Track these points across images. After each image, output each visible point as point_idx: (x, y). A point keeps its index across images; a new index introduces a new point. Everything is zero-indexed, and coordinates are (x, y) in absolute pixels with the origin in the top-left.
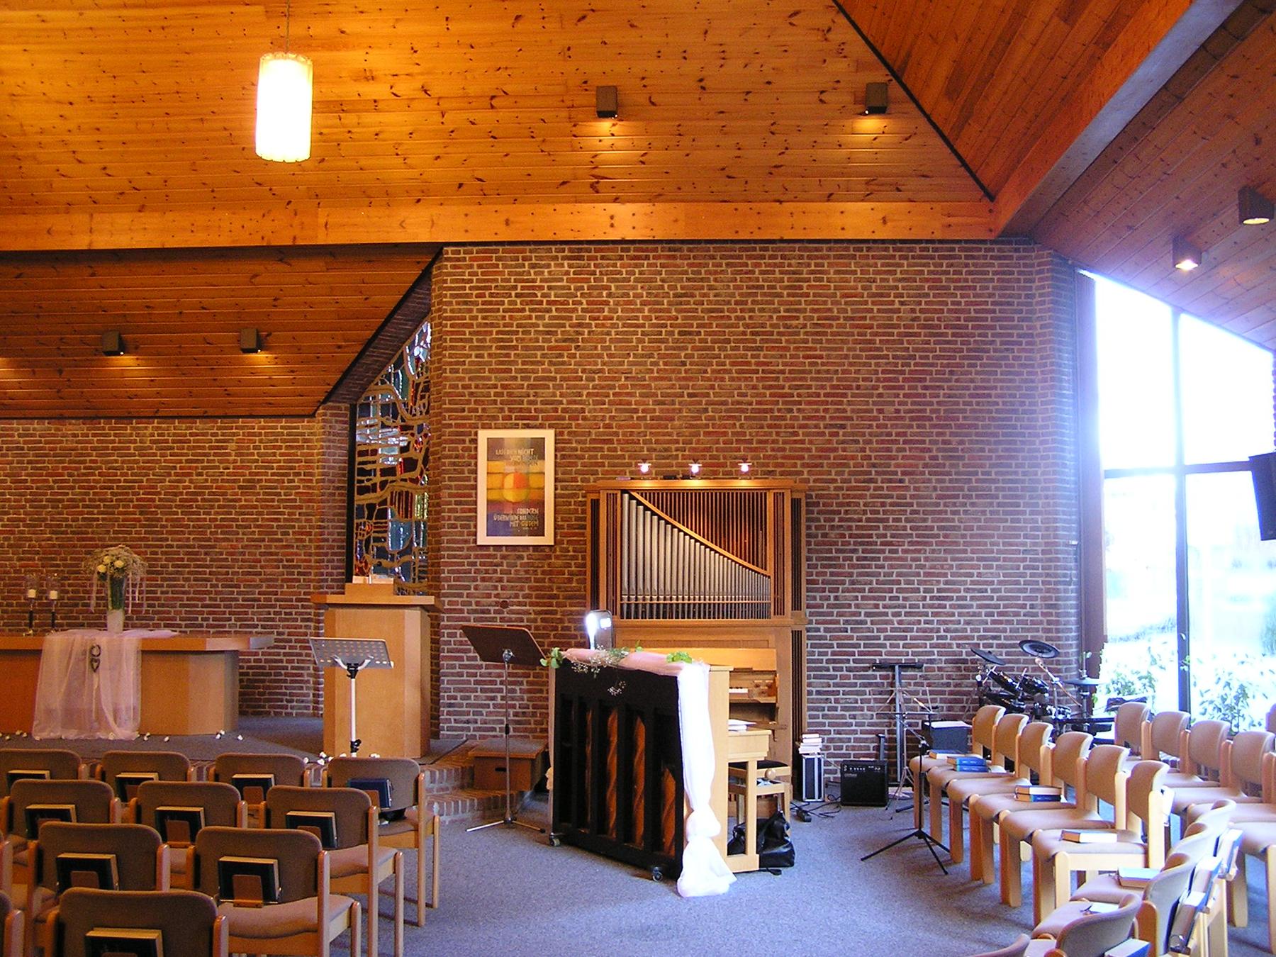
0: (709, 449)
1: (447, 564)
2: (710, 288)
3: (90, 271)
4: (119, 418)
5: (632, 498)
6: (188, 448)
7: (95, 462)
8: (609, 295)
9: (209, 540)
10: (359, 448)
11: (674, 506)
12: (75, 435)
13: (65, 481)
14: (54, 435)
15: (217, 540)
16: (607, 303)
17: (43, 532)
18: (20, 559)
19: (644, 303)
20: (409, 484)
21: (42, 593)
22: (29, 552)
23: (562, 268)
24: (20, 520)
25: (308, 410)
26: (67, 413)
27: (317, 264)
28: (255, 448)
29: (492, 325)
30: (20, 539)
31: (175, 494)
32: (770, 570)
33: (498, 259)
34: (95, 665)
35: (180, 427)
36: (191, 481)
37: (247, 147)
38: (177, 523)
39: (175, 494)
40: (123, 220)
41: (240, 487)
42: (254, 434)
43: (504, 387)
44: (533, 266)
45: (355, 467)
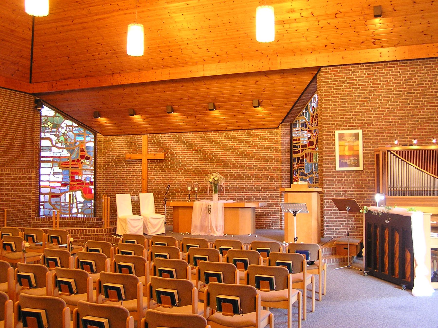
3: (204, 83)
5: (391, 153)
7: (207, 145)
8: (381, 81)
9: (245, 170)
11: (407, 156)
12: (201, 137)
13: (198, 152)
14: (194, 137)
18: (185, 178)
19: (393, 83)
23: (362, 73)
25: (276, 126)
26: (197, 130)
27: (278, 76)
30: (185, 171)
31: (233, 156)
36: (238, 151)
39: (233, 156)
41: (254, 153)
42: (258, 135)
43: (344, 115)
44: (353, 73)
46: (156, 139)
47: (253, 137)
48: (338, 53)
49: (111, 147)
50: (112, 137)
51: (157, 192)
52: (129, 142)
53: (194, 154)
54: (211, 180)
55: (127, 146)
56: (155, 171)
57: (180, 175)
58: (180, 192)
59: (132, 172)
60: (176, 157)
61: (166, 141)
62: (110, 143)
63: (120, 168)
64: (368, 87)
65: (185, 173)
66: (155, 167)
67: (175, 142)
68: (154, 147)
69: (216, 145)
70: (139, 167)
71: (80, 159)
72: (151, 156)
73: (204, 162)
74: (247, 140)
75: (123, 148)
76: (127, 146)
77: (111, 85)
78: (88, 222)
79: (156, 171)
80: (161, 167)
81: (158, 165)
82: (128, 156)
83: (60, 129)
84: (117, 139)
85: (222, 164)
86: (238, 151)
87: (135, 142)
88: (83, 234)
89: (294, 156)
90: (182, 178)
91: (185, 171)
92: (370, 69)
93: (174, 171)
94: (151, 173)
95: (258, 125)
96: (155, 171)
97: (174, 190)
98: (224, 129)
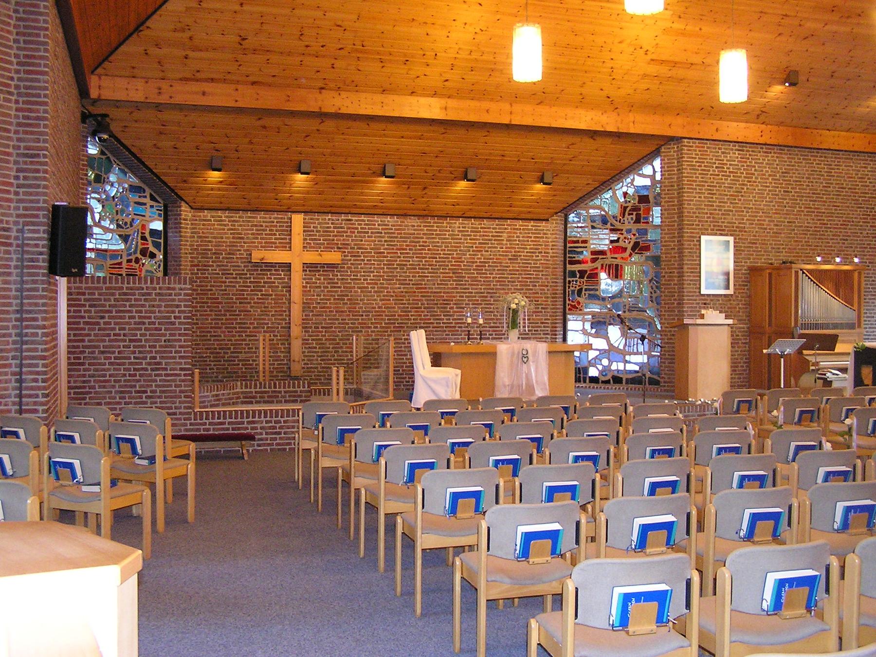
0: (795, 249)
1: (687, 304)
2: (797, 170)
3: (444, 131)
4: (440, 217)
5: (803, 273)
6: (480, 236)
7: (426, 242)
8: (755, 170)
9: (493, 289)
10: (569, 239)
11: (820, 277)
12: (413, 226)
13: (407, 253)
14: (400, 226)
15: (497, 289)
16: (753, 174)
17: (395, 284)
18: (381, 300)
19: (770, 175)
20: (622, 261)
21: (475, 320)
22: (387, 296)
23: (734, 155)
24: (381, 276)
25: (546, 217)
26: (410, 213)
27: (608, 141)
28: (518, 237)
29: (706, 182)
30: (381, 288)
31: (473, 262)
32: (856, 307)
33: (708, 148)
34: (525, 360)
35: (476, 223)
36: (482, 255)
37: (717, 97)
38: (474, 279)
39: (473, 262)
40: (528, 108)
41: (510, 259)
42: (517, 229)
43: (711, 214)
44: (723, 153)
45: (570, 249)
46: (319, 224)
47: (508, 233)
48: (711, 121)
49: (212, 233)
50: (214, 213)
51: (322, 328)
52: (256, 226)
53: (399, 257)
54: (513, 306)
55: (252, 234)
56: (317, 287)
57: (371, 296)
58: (370, 327)
59: (264, 287)
60: (363, 260)
61: (342, 228)
62: (209, 225)
63: (236, 278)
64: (740, 177)
65: (381, 292)
66: (319, 279)
67: (361, 232)
68: (315, 239)
69: (443, 243)
70: (280, 279)
71: (140, 257)
72: (312, 257)
73: (418, 273)
74: (497, 238)
75: (242, 238)
76: (252, 234)
77: (317, 110)
78: (285, 392)
79: (320, 287)
80: (331, 279)
81: (324, 275)
82: (257, 256)
83: (108, 188)
84: (227, 217)
85: (451, 277)
86: (482, 255)
87: (271, 226)
88: (246, 420)
89: (570, 267)
90: (375, 300)
91: (381, 288)
92: (743, 151)
93: (359, 288)
94: (310, 291)
95: (521, 212)
96: (317, 287)
97: (359, 323)
98: (460, 214)
